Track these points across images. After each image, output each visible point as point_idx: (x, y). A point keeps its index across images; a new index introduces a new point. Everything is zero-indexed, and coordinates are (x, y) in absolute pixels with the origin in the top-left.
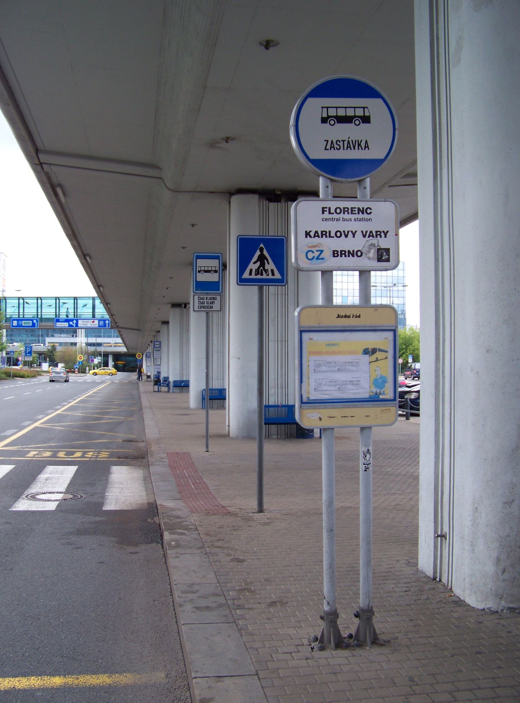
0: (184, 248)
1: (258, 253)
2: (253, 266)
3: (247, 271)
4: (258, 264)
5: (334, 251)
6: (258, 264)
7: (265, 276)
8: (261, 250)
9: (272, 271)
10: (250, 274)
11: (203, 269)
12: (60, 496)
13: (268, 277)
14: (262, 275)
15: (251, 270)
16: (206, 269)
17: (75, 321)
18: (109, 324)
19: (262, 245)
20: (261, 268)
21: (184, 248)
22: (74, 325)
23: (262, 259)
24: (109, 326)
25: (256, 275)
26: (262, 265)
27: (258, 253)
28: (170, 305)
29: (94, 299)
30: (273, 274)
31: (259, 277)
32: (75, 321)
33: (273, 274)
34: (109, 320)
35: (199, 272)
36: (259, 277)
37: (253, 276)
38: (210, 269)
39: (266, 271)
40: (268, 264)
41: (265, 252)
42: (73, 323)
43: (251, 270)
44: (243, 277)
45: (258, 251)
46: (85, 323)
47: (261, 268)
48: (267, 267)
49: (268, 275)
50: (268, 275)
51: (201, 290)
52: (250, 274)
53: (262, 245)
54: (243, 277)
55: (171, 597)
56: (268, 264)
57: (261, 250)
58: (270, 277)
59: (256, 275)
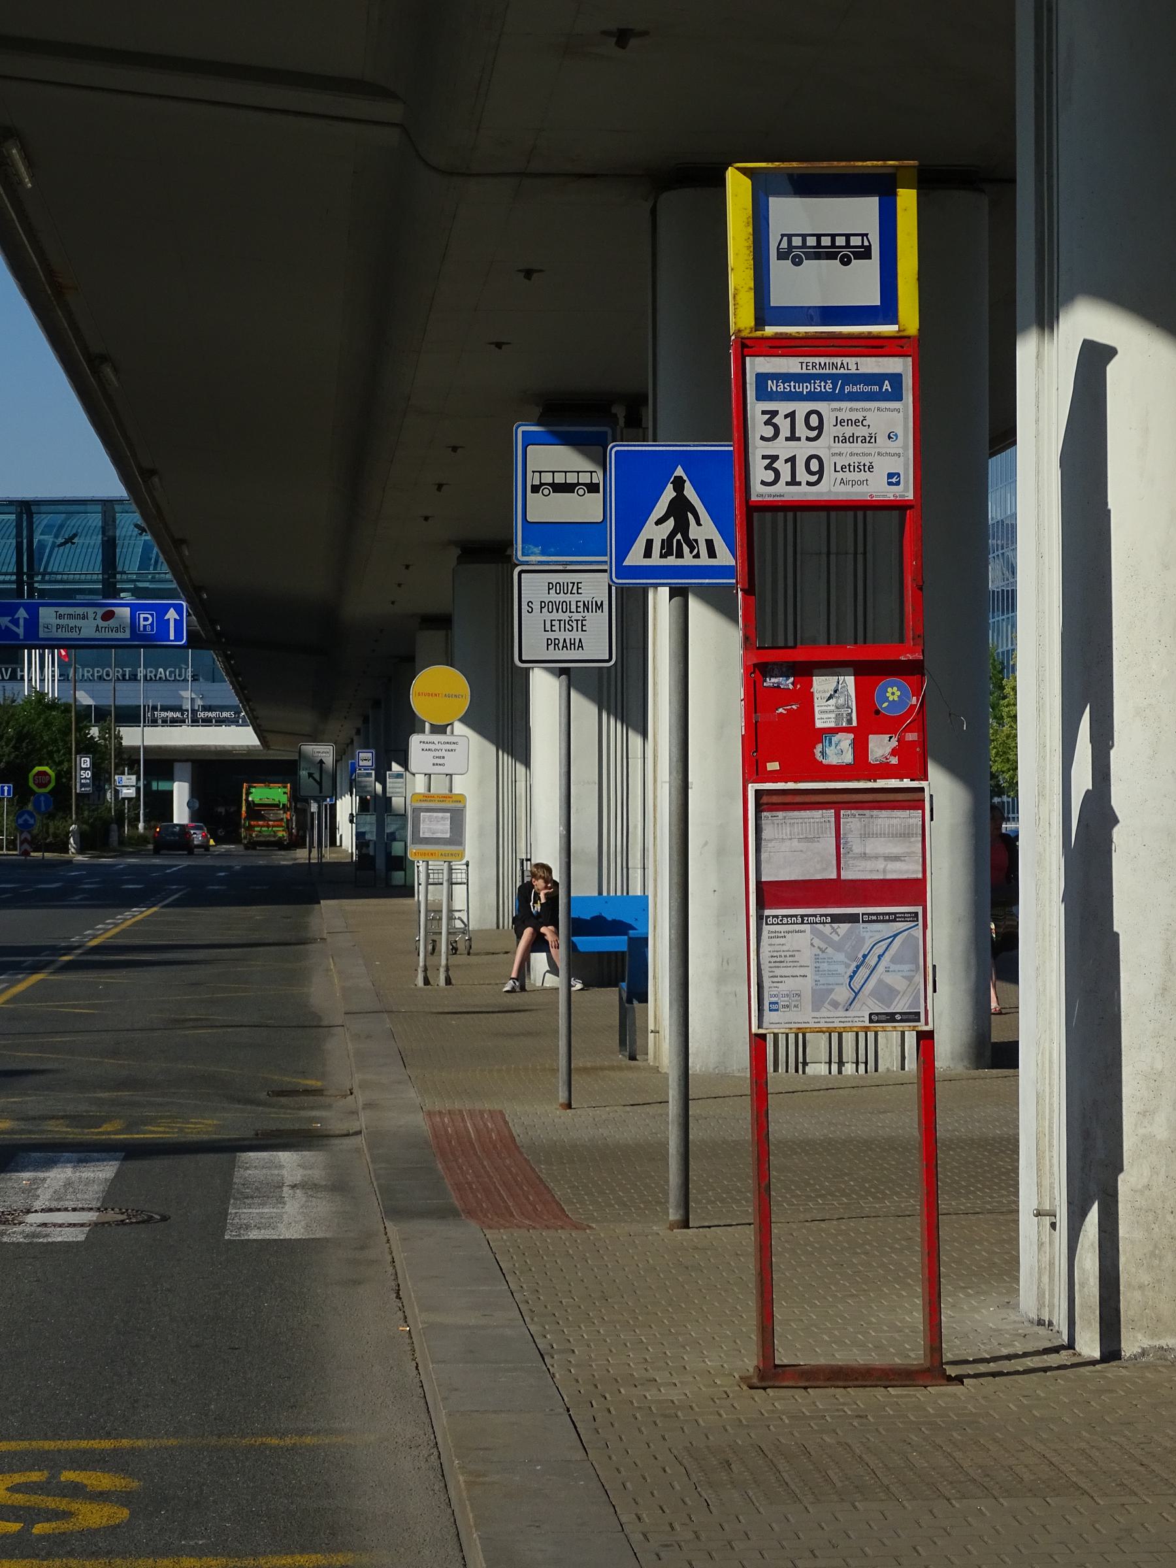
0: (499, 345)
1: (669, 493)
2: (655, 531)
3: (639, 546)
4: (671, 523)
5: (890, 484)
6: (671, 523)
7: (688, 560)
8: (679, 484)
9: (710, 544)
10: (648, 554)
11: (547, 478)
12: (92, 1216)
13: (696, 562)
14: (680, 555)
15: (649, 543)
16: (559, 479)
17: (22, 614)
18: (178, 623)
19: (679, 472)
20: (679, 536)
21: (499, 345)
22: (21, 631)
23: (680, 510)
24: (178, 636)
25: (662, 556)
26: (682, 527)
27: (669, 493)
28: (455, 552)
29: (108, 506)
30: (712, 553)
31: (671, 561)
32: (22, 614)
33: (712, 553)
34: (179, 609)
35: (535, 489)
36: (671, 561)
37: (656, 560)
38: (572, 479)
39: (692, 544)
40: (699, 524)
41: (689, 492)
42: (16, 622)
43: (649, 543)
44: (628, 562)
45: (670, 486)
46: (72, 623)
47: (679, 536)
48: (694, 532)
49: (697, 556)
50: (697, 556)
51: (543, 553)
52: (648, 554)
53: (679, 472)
54: (628, 562)
55: (400, 1314)
56: (699, 524)
57: (679, 484)
58: (704, 560)
59: (662, 556)
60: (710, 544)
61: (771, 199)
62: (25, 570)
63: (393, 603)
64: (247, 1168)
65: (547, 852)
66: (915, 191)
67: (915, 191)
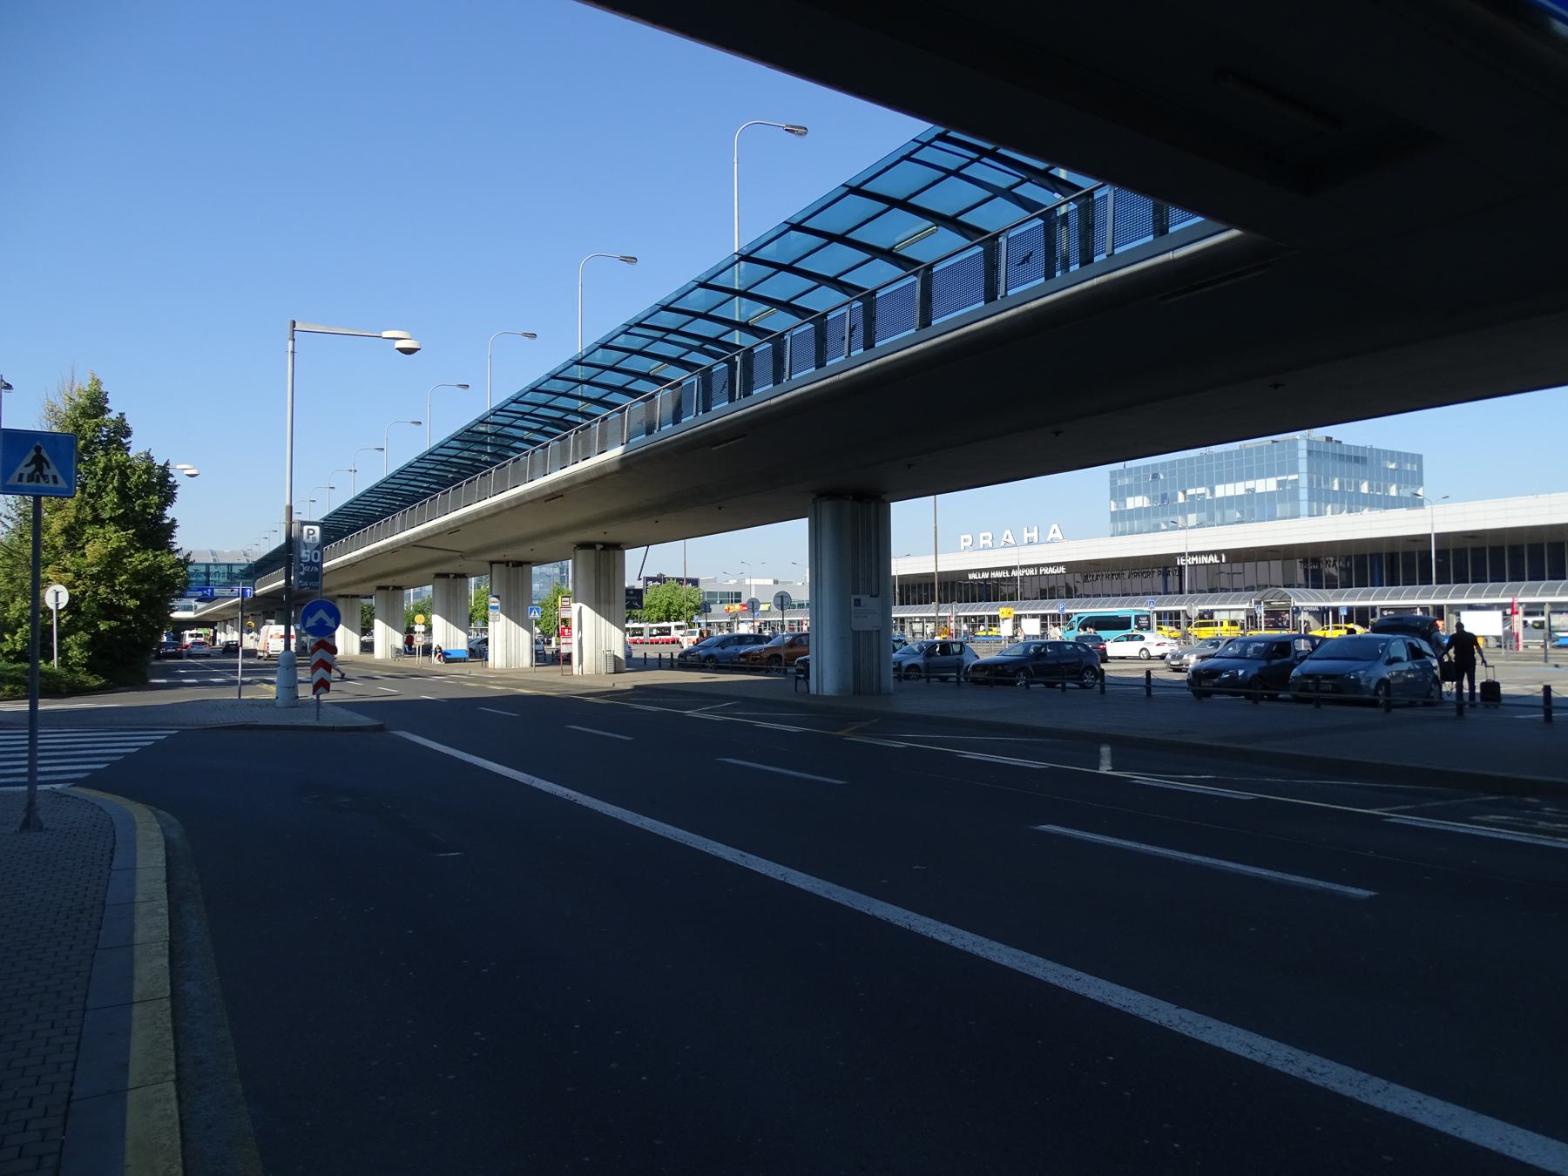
8: (38, 449)
9: (55, 478)
10: (20, 479)
15: (21, 475)
26: (40, 469)
30: (55, 481)
33: (55, 481)
36: (32, 484)
37: (24, 483)
39: (45, 477)
43: (21, 475)
52: (20, 479)
60: (55, 478)
61: (801, 526)
62: (45, 705)
63: (1276, 386)
64: (242, 606)
65: (1151, 238)
66: (897, 509)
67: (897, 509)
